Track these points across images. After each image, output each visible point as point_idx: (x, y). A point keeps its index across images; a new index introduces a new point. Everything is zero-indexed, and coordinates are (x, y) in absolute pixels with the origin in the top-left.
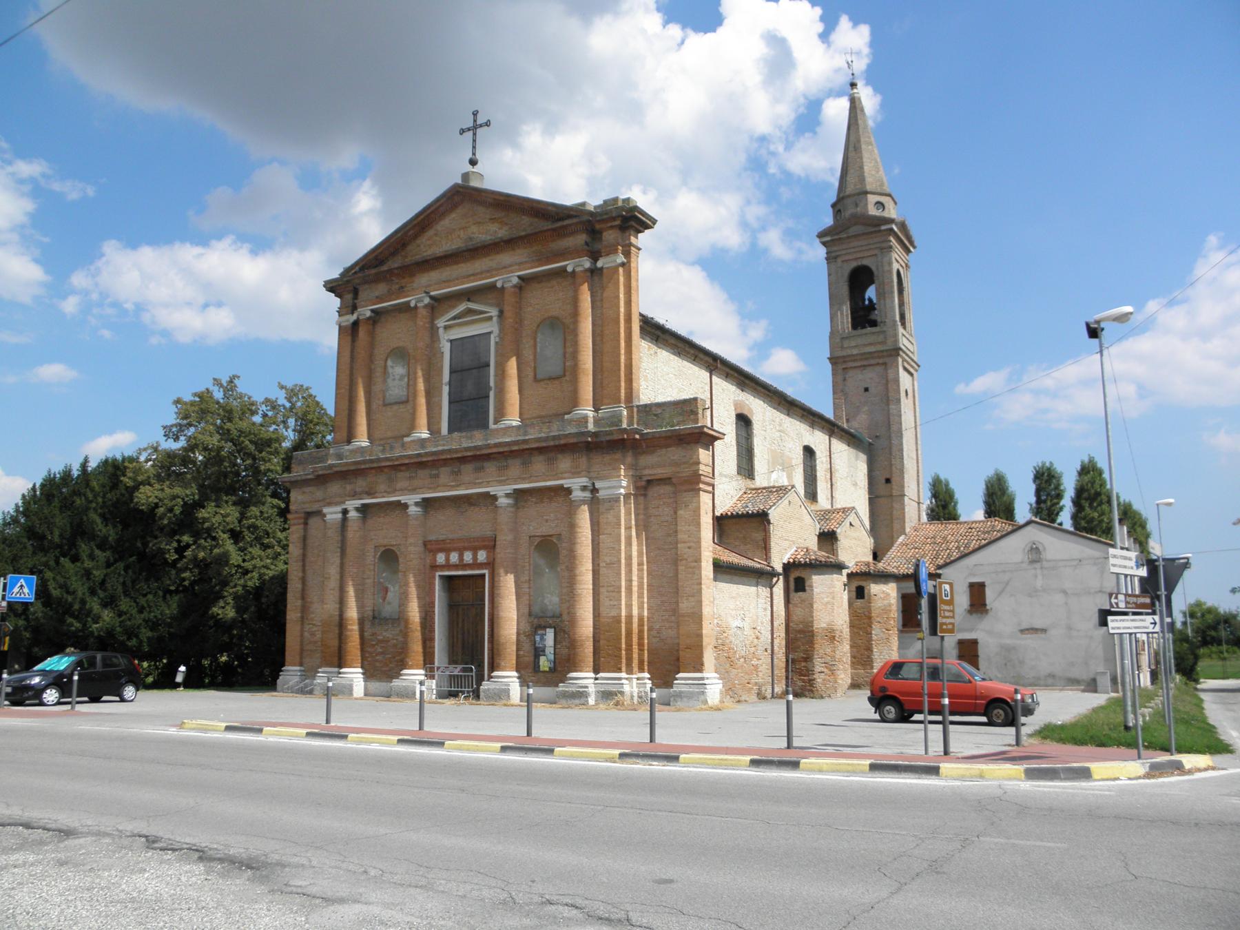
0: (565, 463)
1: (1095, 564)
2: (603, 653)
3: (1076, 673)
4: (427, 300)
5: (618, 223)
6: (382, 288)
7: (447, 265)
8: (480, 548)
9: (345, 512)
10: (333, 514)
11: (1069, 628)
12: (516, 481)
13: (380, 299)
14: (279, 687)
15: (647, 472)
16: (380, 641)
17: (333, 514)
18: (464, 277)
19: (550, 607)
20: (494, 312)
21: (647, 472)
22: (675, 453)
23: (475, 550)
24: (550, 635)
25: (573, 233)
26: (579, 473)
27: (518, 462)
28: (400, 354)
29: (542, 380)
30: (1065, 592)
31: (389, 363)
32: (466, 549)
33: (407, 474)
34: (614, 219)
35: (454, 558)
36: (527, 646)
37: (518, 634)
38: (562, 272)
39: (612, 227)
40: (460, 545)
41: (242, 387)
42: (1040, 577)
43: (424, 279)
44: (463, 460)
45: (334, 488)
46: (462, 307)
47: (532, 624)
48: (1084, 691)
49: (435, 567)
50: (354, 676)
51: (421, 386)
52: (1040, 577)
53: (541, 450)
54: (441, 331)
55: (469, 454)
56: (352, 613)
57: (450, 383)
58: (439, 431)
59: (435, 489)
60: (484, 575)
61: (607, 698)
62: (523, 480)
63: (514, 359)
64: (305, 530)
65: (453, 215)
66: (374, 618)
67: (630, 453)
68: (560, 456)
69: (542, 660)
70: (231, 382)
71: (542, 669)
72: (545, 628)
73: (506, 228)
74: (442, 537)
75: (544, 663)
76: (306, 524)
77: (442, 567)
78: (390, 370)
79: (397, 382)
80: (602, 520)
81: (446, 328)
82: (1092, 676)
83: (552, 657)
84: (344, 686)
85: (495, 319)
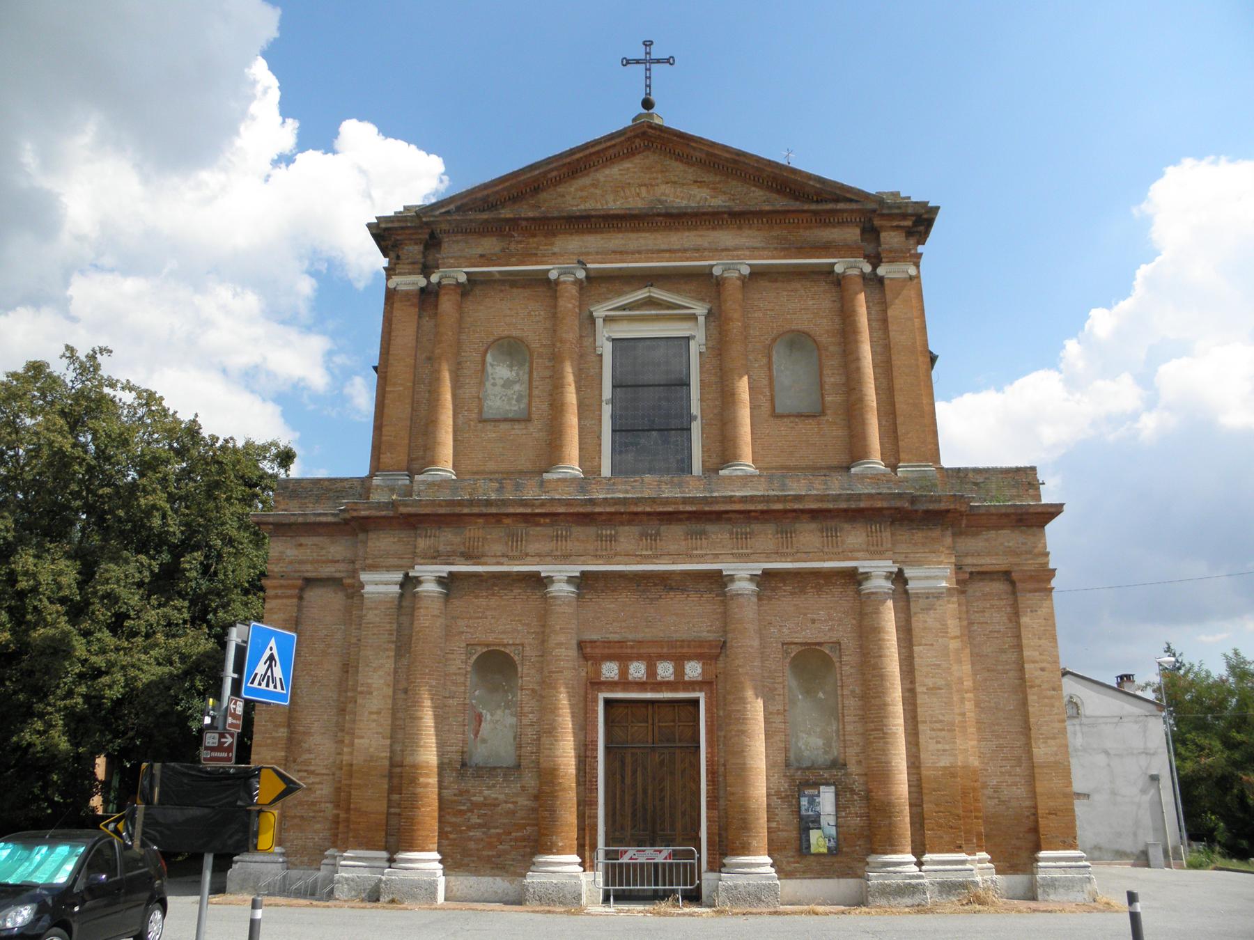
0: (855, 537)
1: (1136, 722)
2: (928, 824)
3: (1128, 845)
4: (581, 274)
5: (908, 223)
6: (489, 245)
7: (619, 230)
8: (690, 658)
9: (409, 583)
10: (380, 585)
11: (1114, 793)
12: (768, 557)
13: (485, 259)
14: (229, 885)
15: (969, 560)
16: (476, 805)
17: (380, 585)
18: (653, 252)
19: (806, 753)
20: (700, 309)
21: (969, 560)
22: (1009, 539)
23: (679, 661)
24: (827, 799)
25: (842, 224)
26: (881, 553)
27: (770, 528)
28: (512, 349)
29: (782, 416)
30: (1107, 753)
31: (489, 358)
32: (662, 657)
33: (550, 531)
34: (904, 216)
35: (637, 670)
36: (784, 814)
37: (768, 796)
38: (828, 272)
39: (898, 227)
40: (654, 650)
41: (107, 367)
42: (1079, 735)
43: (574, 243)
44: (670, 517)
45: (383, 542)
46: (641, 294)
47: (792, 779)
48: (1134, 865)
49: (597, 684)
50: (426, 863)
51: (571, 397)
52: (1079, 735)
53: (815, 515)
54: (599, 322)
55: (689, 508)
56: (429, 755)
57: (613, 401)
58: (598, 471)
59: (609, 560)
60: (696, 702)
61: (949, 893)
62: (781, 556)
63: (746, 378)
64: (300, 608)
65: (627, 165)
66: (464, 765)
67: (949, 533)
68: (847, 526)
69: (815, 835)
70: (92, 357)
71: (813, 850)
72: (816, 785)
73: (723, 197)
74: (616, 637)
75: (818, 841)
76: (301, 598)
77: (611, 685)
78: (489, 369)
79: (498, 389)
80: (916, 624)
81: (607, 320)
82: (1141, 847)
83: (833, 831)
84: (416, 885)
85: (701, 320)
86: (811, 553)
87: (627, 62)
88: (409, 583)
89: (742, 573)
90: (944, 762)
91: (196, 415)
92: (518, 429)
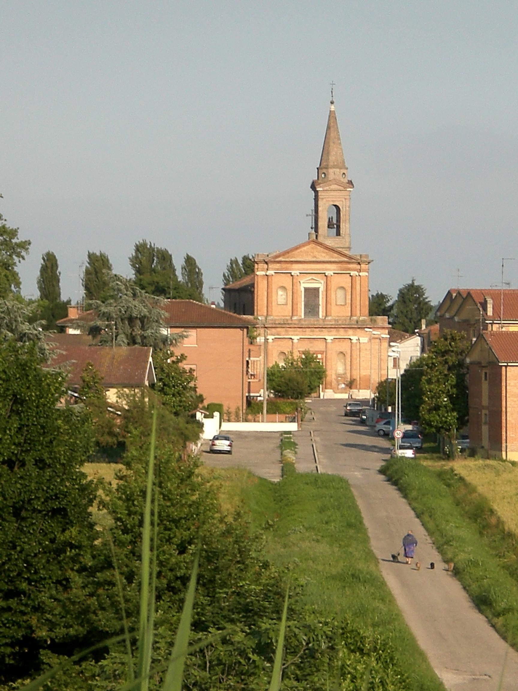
0: (351, 332)
57: (304, 301)
86: (342, 334)
87: (307, 215)
88: (266, 340)
89: (329, 338)
90: (364, 374)
91: (18, 228)
92: (285, 306)
